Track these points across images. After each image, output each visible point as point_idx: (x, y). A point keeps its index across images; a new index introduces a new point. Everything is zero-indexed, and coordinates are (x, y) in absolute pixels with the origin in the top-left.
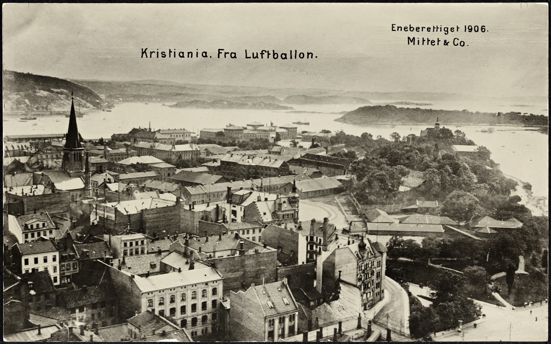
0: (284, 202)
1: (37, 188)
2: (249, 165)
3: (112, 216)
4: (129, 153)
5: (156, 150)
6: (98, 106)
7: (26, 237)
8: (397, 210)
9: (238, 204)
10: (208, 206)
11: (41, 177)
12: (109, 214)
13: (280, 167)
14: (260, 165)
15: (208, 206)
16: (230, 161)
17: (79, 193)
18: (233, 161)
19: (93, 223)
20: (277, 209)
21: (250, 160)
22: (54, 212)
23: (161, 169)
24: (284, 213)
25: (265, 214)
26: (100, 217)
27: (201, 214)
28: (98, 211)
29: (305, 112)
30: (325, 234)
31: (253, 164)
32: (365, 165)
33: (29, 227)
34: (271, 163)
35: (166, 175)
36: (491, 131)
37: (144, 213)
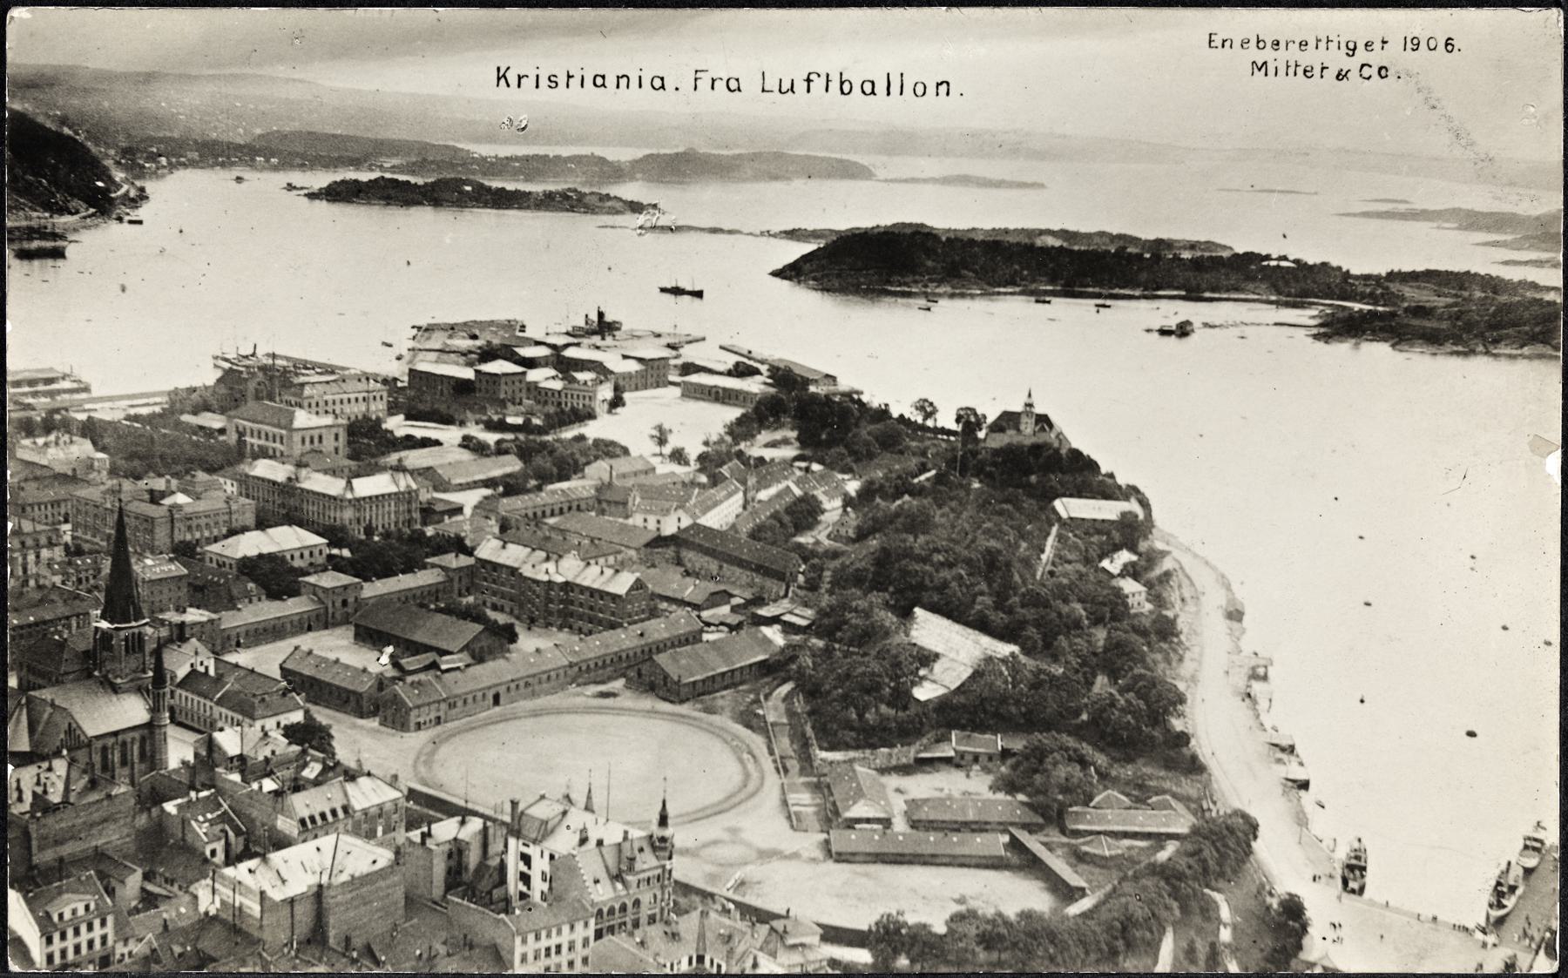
0: (641, 850)
1: (50, 769)
2: (550, 582)
3: (254, 908)
4: (234, 507)
5: (302, 490)
6: (103, 205)
7: (49, 941)
8: (904, 760)
9: (535, 842)
10: (463, 823)
11: (49, 710)
12: (246, 902)
13: (628, 593)
14: (578, 581)
15: (463, 823)
16: (500, 560)
17: (137, 735)
18: (509, 563)
19: (207, 913)
20: (624, 868)
21: (551, 566)
22: (100, 842)
23: (325, 590)
24: (642, 876)
25: (597, 882)
26: (223, 902)
27: (446, 848)
28: (217, 886)
29: (690, 228)
30: (731, 952)
31: (560, 579)
32: (856, 413)
33: (56, 918)
34: (603, 579)
35: (338, 604)
36: (1183, 330)
37: (326, 893)
